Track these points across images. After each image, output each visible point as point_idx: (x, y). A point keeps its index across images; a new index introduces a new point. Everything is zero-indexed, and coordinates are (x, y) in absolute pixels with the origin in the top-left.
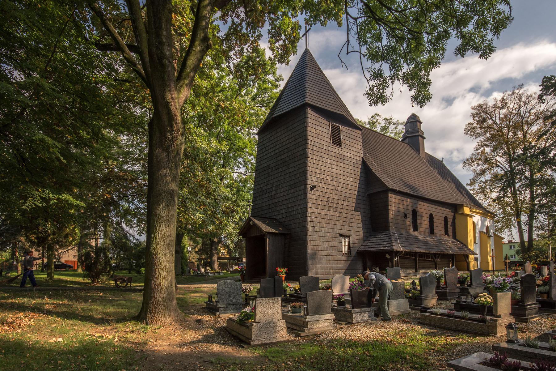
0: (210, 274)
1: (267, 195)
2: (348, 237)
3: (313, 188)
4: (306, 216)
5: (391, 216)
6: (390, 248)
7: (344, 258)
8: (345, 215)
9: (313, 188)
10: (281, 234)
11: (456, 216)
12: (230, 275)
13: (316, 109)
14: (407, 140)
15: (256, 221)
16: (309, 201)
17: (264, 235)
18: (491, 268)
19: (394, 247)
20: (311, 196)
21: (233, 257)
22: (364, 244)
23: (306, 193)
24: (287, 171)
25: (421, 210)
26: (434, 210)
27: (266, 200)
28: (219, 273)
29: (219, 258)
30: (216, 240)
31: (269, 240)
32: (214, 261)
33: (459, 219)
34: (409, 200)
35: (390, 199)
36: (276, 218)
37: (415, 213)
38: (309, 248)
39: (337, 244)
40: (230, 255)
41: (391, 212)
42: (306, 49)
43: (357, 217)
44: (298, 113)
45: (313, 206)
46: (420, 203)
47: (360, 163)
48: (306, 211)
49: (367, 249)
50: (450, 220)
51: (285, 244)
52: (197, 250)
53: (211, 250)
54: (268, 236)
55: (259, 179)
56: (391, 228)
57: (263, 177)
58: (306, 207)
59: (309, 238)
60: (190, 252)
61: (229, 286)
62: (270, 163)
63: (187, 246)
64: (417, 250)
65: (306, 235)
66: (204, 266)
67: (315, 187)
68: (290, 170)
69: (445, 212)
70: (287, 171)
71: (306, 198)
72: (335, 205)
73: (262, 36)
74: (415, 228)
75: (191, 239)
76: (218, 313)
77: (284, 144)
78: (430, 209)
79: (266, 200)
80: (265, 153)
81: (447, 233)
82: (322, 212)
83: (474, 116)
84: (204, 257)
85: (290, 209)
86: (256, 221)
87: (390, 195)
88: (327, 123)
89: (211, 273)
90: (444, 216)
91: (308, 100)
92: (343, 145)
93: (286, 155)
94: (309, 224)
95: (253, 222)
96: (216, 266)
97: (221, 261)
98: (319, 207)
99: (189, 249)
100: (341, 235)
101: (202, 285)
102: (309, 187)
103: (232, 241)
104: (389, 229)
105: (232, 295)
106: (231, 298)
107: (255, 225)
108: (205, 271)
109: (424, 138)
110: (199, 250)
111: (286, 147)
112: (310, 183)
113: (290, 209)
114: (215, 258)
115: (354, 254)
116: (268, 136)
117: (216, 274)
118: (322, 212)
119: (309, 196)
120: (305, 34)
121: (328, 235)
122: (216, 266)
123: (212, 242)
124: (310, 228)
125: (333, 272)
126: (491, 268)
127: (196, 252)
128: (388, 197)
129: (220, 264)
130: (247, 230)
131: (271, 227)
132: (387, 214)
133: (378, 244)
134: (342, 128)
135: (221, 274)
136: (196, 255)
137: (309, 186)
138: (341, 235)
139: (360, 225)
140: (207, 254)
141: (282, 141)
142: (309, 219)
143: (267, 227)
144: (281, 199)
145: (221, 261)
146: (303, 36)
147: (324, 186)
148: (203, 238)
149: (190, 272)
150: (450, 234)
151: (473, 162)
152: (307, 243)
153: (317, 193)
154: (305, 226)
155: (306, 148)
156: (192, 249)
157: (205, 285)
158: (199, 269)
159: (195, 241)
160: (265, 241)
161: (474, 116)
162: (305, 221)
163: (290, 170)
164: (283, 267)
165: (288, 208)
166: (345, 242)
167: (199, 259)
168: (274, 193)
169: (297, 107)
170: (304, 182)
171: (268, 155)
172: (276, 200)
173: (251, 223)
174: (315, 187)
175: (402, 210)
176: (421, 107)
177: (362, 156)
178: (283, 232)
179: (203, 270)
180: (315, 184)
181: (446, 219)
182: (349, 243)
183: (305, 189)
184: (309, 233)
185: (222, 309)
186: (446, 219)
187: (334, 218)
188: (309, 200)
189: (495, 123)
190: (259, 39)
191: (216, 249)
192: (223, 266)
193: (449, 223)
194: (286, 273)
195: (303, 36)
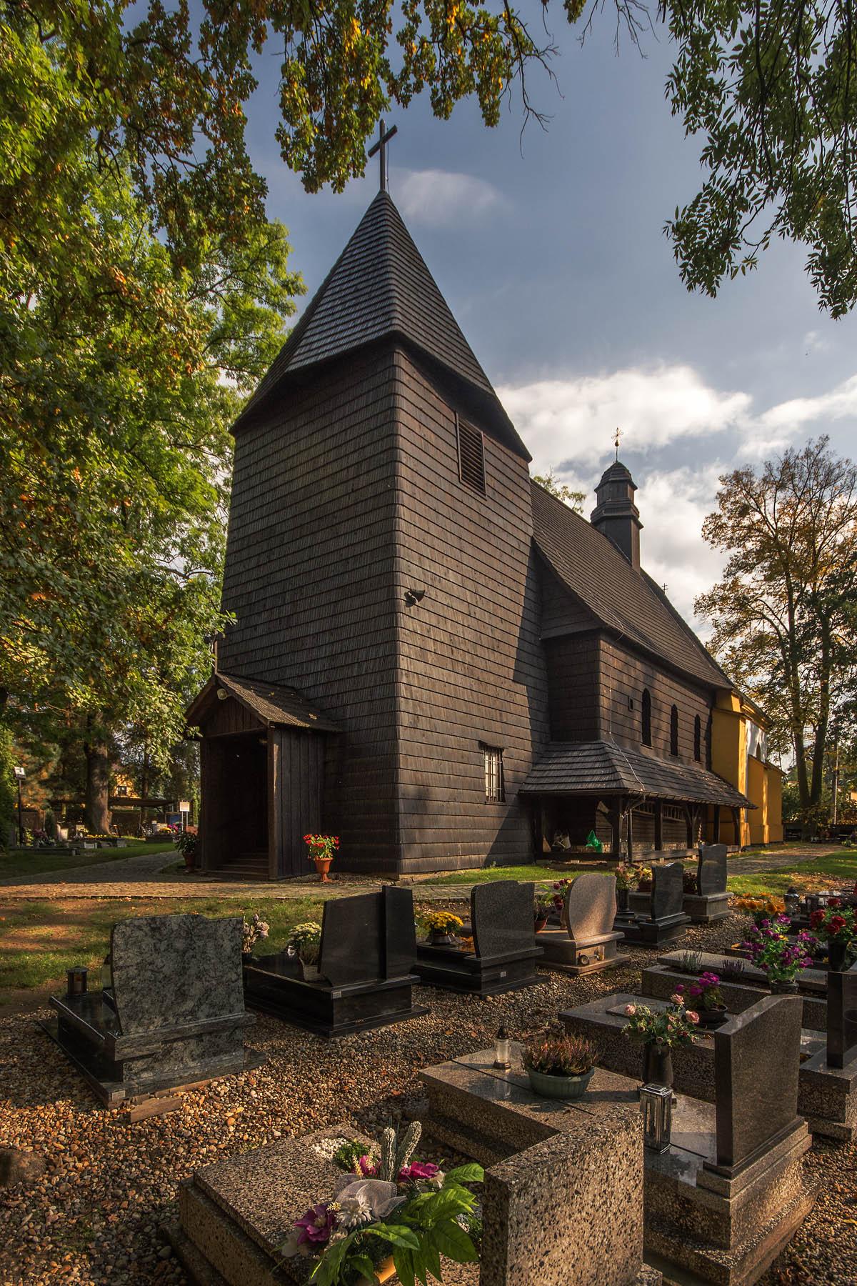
0: (86, 845)
1: (265, 616)
2: (498, 751)
3: (415, 597)
4: (394, 683)
5: (605, 702)
6: (614, 785)
7: (493, 809)
8: (491, 690)
9: (415, 597)
10: (314, 734)
11: (716, 717)
12: (146, 846)
13: (422, 360)
14: (603, 527)
15: (238, 688)
16: (402, 637)
17: (264, 733)
18: (766, 840)
19: (627, 784)
20: (410, 622)
21: (150, 801)
22: (535, 774)
23: (393, 613)
24: (332, 545)
25: (660, 696)
26: (679, 696)
27: (261, 630)
28: (114, 841)
29: (113, 801)
30: (104, 751)
31: (280, 749)
32: (102, 810)
33: (720, 723)
34: (639, 665)
35: (603, 655)
36: (296, 684)
37: (647, 698)
38: (405, 776)
39: (471, 769)
40: (143, 795)
41: (603, 690)
42: (382, 192)
43: (519, 699)
44: (373, 358)
45: (413, 652)
46: (660, 677)
47: (527, 550)
48: (395, 667)
49: (546, 788)
50: (704, 725)
51: (325, 763)
52: (45, 775)
53: (89, 781)
54: (276, 737)
55: (240, 568)
56: (603, 733)
57: (253, 563)
58: (394, 654)
59: (403, 747)
60: (23, 782)
61: (180, 945)
62: (273, 520)
63: (12, 762)
64: (670, 793)
65: (396, 737)
66: (69, 823)
67: (420, 596)
68: (342, 542)
69: (696, 705)
70: (332, 545)
71: (393, 627)
72: (468, 658)
73: (254, 84)
74: (647, 741)
75: (25, 745)
76: (118, 1095)
77: (321, 461)
78: (673, 693)
79: (261, 630)
80: (259, 490)
81: (698, 758)
82: (436, 673)
83: (722, 498)
84: (67, 797)
85: (342, 660)
86: (238, 688)
87: (603, 644)
88: (451, 416)
89: (90, 841)
90: (695, 713)
91: (398, 324)
92: (488, 491)
93: (327, 496)
94: (403, 704)
95: (228, 690)
96: (106, 823)
97: (119, 808)
98: (431, 658)
99: (20, 771)
100: (484, 746)
101: (55, 890)
102: (402, 592)
103: (164, 743)
104: (597, 737)
105: (196, 989)
106: (189, 1005)
107: (234, 700)
108: (71, 834)
109: (640, 526)
110: (53, 778)
111: (329, 470)
112: (406, 583)
113: (342, 660)
114: (103, 799)
115: (512, 798)
116: (268, 438)
117: (104, 844)
118: (436, 673)
119: (404, 621)
120: (379, 148)
121: (452, 741)
122: (106, 823)
123: (93, 758)
124: (405, 719)
125: (463, 849)
126: (766, 840)
127: (43, 783)
128: (597, 649)
129: (116, 817)
130: (208, 711)
131: (285, 708)
132: (596, 695)
133: (577, 772)
134: (487, 442)
135: (121, 845)
136: (42, 791)
137: (404, 591)
138: (484, 746)
139: (526, 722)
140: (79, 789)
141: (313, 452)
142: (403, 690)
143: (273, 707)
144: (312, 629)
145: (119, 808)
146: (371, 154)
147: (442, 597)
148: (65, 744)
149: (22, 839)
150: (703, 757)
151: (714, 603)
152: (396, 761)
153: (425, 616)
154: (393, 712)
155: (395, 475)
156: (28, 773)
157: (66, 889)
158: (52, 831)
159: (36, 750)
160: (265, 752)
161: (722, 498)
162: (393, 697)
163: (342, 542)
164: (325, 832)
165: (333, 656)
166: (490, 764)
167: (55, 804)
168: (287, 610)
169: (366, 344)
170: (388, 578)
171: (269, 497)
172: (295, 633)
173: (220, 694)
174: (420, 596)
175: (628, 690)
176: (836, 314)
177: (531, 532)
178: (321, 727)
179: (64, 833)
180: (420, 587)
181: (697, 719)
182: (501, 768)
183: (392, 599)
184: (403, 733)
185: (140, 1064)
186: (697, 719)
187: (466, 695)
188: (403, 635)
189: (765, 520)
190: (244, 96)
191: (104, 775)
192: (125, 822)
193: (703, 733)
194: (333, 851)
195: (371, 154)
